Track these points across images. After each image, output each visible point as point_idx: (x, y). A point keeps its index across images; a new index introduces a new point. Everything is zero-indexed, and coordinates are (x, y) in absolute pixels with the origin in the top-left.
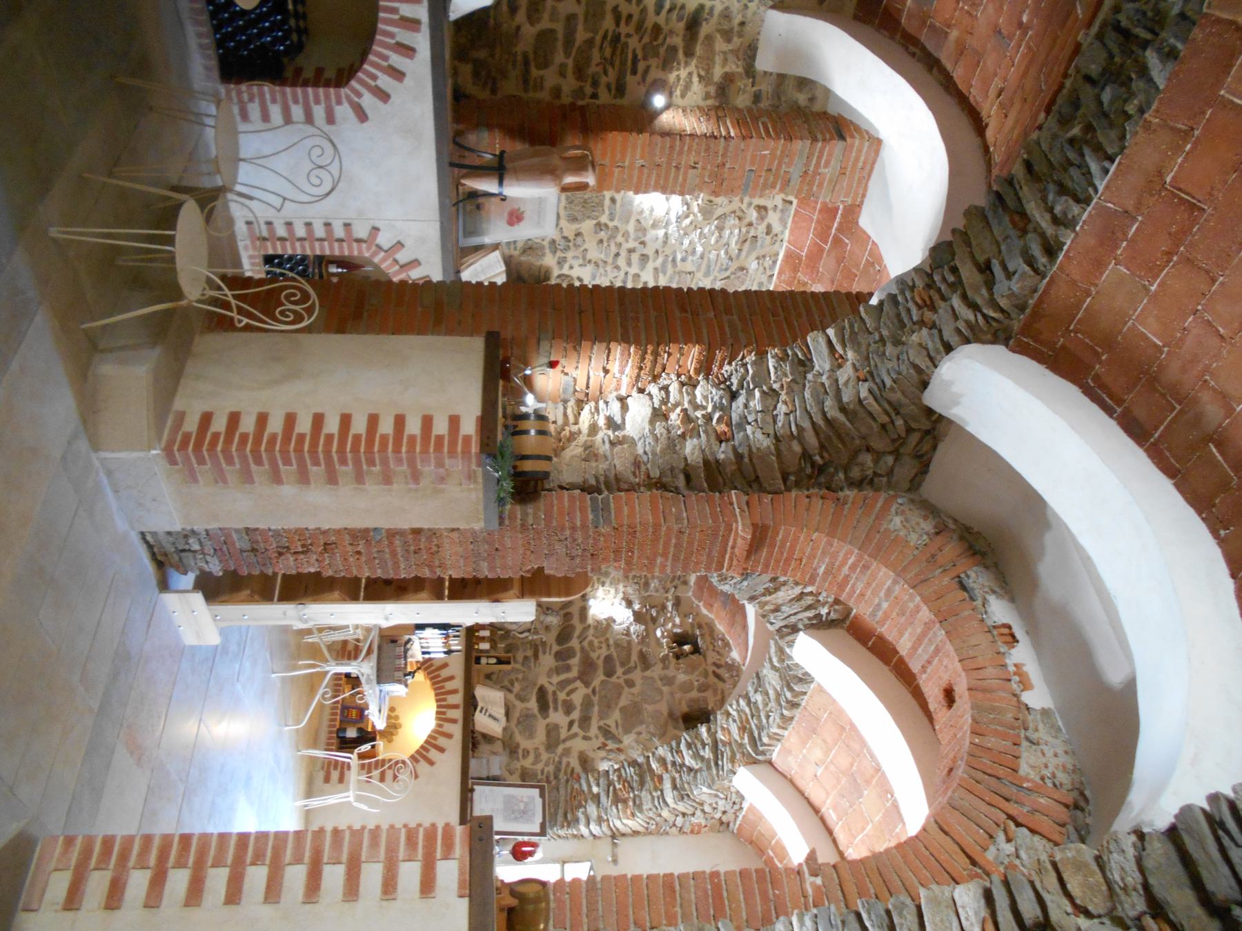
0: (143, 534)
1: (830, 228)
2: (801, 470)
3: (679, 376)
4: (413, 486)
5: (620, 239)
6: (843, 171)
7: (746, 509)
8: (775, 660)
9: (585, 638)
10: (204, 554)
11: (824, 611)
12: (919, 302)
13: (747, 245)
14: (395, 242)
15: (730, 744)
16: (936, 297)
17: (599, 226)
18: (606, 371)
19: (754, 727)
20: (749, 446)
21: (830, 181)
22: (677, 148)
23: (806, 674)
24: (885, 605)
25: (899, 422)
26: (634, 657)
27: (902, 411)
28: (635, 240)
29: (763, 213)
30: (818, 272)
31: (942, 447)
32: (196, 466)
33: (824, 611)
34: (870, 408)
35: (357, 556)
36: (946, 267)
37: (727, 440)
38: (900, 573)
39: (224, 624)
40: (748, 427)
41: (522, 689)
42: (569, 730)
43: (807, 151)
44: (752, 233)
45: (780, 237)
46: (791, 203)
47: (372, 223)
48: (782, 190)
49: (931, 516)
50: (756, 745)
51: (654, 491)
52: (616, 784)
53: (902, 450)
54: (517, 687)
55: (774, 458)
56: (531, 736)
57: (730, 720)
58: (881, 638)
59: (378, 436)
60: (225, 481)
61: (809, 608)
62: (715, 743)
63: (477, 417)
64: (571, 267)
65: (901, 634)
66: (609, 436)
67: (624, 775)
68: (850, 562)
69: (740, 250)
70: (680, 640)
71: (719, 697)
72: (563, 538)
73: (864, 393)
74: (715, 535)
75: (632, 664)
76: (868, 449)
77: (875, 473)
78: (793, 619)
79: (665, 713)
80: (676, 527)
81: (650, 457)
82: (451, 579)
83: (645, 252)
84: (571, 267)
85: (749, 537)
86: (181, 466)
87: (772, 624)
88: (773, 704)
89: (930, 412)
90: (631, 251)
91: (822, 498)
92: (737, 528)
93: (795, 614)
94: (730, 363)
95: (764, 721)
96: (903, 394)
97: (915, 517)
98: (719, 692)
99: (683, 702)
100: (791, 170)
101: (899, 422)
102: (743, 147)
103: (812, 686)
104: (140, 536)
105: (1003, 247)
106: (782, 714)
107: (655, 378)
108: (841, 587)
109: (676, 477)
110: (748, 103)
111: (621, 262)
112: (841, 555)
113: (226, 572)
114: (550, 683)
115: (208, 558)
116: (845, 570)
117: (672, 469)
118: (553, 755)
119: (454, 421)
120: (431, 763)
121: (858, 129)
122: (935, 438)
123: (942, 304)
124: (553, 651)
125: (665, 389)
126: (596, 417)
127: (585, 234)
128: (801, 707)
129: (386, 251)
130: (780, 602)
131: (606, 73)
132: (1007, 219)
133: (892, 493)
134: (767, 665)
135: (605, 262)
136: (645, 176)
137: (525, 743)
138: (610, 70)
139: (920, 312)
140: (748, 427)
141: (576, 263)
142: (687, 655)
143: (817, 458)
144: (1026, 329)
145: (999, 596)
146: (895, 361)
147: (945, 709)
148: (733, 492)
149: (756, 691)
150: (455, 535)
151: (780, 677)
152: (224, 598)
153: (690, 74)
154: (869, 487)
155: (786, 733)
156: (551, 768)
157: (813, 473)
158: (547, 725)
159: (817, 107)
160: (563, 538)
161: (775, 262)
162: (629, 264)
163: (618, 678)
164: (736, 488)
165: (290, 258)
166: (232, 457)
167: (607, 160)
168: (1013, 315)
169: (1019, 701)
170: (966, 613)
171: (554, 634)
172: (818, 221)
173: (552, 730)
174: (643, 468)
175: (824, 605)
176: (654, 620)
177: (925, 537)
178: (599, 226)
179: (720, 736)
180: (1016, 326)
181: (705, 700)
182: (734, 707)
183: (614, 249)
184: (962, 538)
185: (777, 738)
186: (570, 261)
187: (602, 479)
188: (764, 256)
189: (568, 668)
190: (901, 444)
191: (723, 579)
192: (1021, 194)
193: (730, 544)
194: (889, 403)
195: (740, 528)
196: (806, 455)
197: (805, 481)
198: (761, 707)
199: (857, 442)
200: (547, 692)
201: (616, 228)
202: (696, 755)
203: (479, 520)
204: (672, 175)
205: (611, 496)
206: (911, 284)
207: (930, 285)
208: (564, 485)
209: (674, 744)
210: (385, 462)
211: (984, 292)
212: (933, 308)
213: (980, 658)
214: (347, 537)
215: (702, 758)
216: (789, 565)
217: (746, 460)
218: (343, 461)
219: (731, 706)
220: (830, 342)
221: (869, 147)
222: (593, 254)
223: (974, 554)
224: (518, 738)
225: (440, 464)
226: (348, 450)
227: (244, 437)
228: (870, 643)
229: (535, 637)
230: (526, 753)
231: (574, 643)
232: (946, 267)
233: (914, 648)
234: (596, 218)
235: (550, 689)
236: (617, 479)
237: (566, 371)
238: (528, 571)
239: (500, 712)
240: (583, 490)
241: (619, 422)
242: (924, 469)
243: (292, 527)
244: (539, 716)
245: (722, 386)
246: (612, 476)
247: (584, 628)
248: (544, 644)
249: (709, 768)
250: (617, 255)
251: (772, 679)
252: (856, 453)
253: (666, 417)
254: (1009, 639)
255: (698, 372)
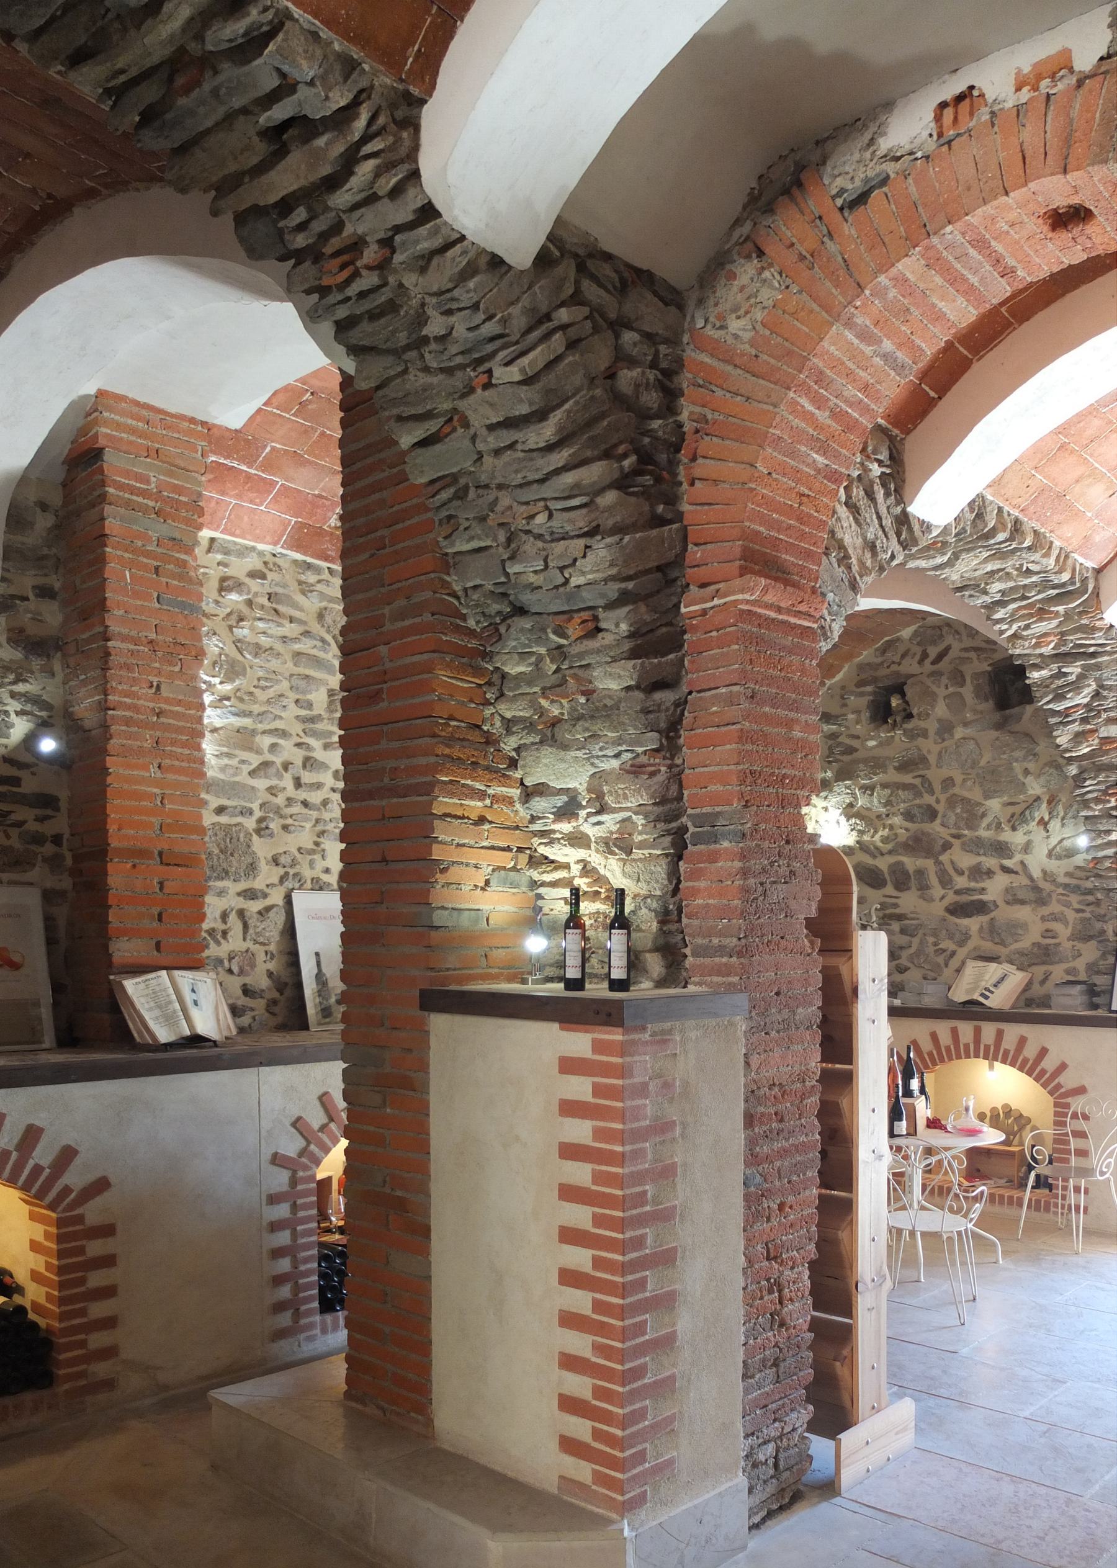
0: (751, 1528)
1: (249, 476)
2: (645, 494)
3: (487, 703)
4: (678, 1130)
5: (280, 800)
6: (153, 454)
7: (713, 588)
8: (939, 560)
9: (877, 848)
10: (780, 1438)
11: (876, 470)
12: (345, 274)
13: (281, 608)
14: (293, 1130)
15: (1063, 634)
16: (335, 243)
17: (262, 830)
18: (482, 820)
19: (1040, 597)
20: (606, 580)
21: (170, 474)
22: (128, 714)
23: (971, 504)
24: (888, 345)
25: (563, 315)
26: (908, 779)
27: (544, 309)
28: (281, 778)
29: (230, 583)
30: (320, 496)
31: (607, 245)
32: (647, 1465)
33: (876, 470)
34: (541, 365)
35: (787, 1209)
36: (281, 224)
37: (596, 618)
38: (834, 314)
39: (886, 1393)
40: (575, 581)
41: (951, 937)
42: (1016, 873)
43: (122, 511)
44: (264, 601)
45: (269, 558)
46: (212, 540)
47: (287, 1123)
48: (189, 550)
49: (728, 267)
50: (1070, 592)
51: (681, 741)
52: (1108, 806)
53: (613, 315)
54: (947, 944)
55: (627, 538)
56: (1024, 926)
57: (1025, 633)
58: (924, 375)
59: (594, 1188)
60: (671, 1419)
61: (870, 495)
62: (1059, 657)
63: (562, 1029)
64: (327, 871)
65: (939, 317)
66: (589, 815)
67: (1095, 795)
68: (809, 407)
69: (292, 620)
70: (881, 714)
71: (973, 655)
72: (760, 889)
73: (514, 373)
74: (758, 640)
75: (917, 781)
76: (611, 376)
77: (654, 365)
78: (888, 522)
79: (994, 734)
80: (745, 705)
81: (624, 748)
82: (822, 1061)
83: (299, 762)
84: (327, 871)
85: (763, 580)
86: (647, 1487)
87: (893, 557)
88: (1009, 565)
89: (543, 260)
90: (298, 783)
91: (694, 459)
92: (748, 602)
93: (879, 518)
94: (464, 618)
95: (1034, 579)
96: (513, 303)
97: (729, 294)
98: (966, 655)
99: (980, 707)
100: (154, 536)
101: (563, 315)
102: (121, 612)
103: (990, 497)
104: (754, 1532)
105: (237, 103)
106: (1029, 548)
107: (490, 740)
108: (850, 426)
109: (659, 705)
110: (54, 606)
111: (315, 797)
112: (796, 422)
113: (808, 1400)
114: (943, 898)
115: (787, 1429)
116: (822, 416)
117: (646, 711)
118: (1054, 896)
119: (569, 1066)
120: (1063, 1067)
121: (83, 431)
122: (591, 255)
123: (349, 229)
124: (895, 893)
125: (509, 724)
126: (558, 836)
127: (274, 852)
128: (1021, 516)
129: (309, 1143)
130: (859, 541)
131: (19, 824)
132: (182, 101)
133: (686, 338)
134: (946, 573)
135: (317, 821)
136: (177, 763)
137: (1033, 936)
138: (14, 817)
139: (364, 272)
140: (575, 581)
141: (320, 865)
142: (907, 703)
143: (626, 463)
144: (392, 60)
145: (881, 131)
146: (453, 319)
147: (1090, 229)
148: (683, 610)
149: (985, 592)
150: (755, 1061)
151: (968, 550)
152: (846, 1398)
153: (13, 695)
154: (675, 379)
155: (1057, 543)
156: (1074, 899)
157: (650, 473)
158: (1007, 903)
159: (56, 499)
160: (760, 889)
161: (309, 566)
162: (319, 786)
163: (938, 801)
164: (677, 606)
165: (322, 1276)
166: (633, 1412)
167: (153, 820)
168: (364, 83)
169: (1091, 76)
170: (913, 189)
171: (870, 893)
172: (239, 496)
173: (1014, 899)
174: (644, 759)
175: (867, 470)
176: (850, 750)
177: (767, 274)
178: (262, 830)
179: (1047, 650)
180: (385, 80)
181: (976, 676)
182: (1005, 627)
183: (296, 809)
184: (769, 209)
185: (1064, 557)
186: (317, 872)
187: (661, 826)
188: (300, 583)
189: (920, 873)
190: (603, 315)
191: (824, 632)
192: (134, 72)
193: (773, 614)
194: (529, 330)
195: (747, 597)
196: (622, 484)
197: (664, 487)
198: (1011, 584)
199: (598, 392)
200: (956, 903)
201: (262, 806)
202: (1076, 686)
203: (732, 1024)
204: (171, 721)
205: (690, 811)
206: (315, 297)
207: (312, 254)
208: (671, 887)
209: (1053, 720)
210: (639, 1178)
211: (321, 142)
212: (357, 245)
213: (1002, 155)
214: (758, 1226)
215: (1081, 677)
216: (810, 516)
217: (630, 585)
218: (638, 1243)
219: (1002, 632)
220: (423, 443)
221: (111, 412)
222: (305, 838)
223: (799, 184)
224: (1025, 944)
225: (642, 1090)
226: (620, 1236)
227: (599, 1393)
228: (932, 394)
229: (874, 919)
230: (1048, 933)
231: (883, 864)
232: (281, 224)
233: (969, 291)
234: (248, 835)
235: (951, 898)
236: (663, 802)
237: (482, 884)
238: (812, 943)
239: (993, 971)
240: (680, 858)
241: (565, 798)
242: (644, 278)
243: (742, 1312)
244: (992, 915)
245: (502, 629)
246: (658, 810)
247: (861, 849)
248: (883, 906)
249: (1098, 667)
250: (305, 804)
251: (970, 565)
252: (619, 399)
253: (555, 722)
254: (965, 105)
255: (478, 671)
